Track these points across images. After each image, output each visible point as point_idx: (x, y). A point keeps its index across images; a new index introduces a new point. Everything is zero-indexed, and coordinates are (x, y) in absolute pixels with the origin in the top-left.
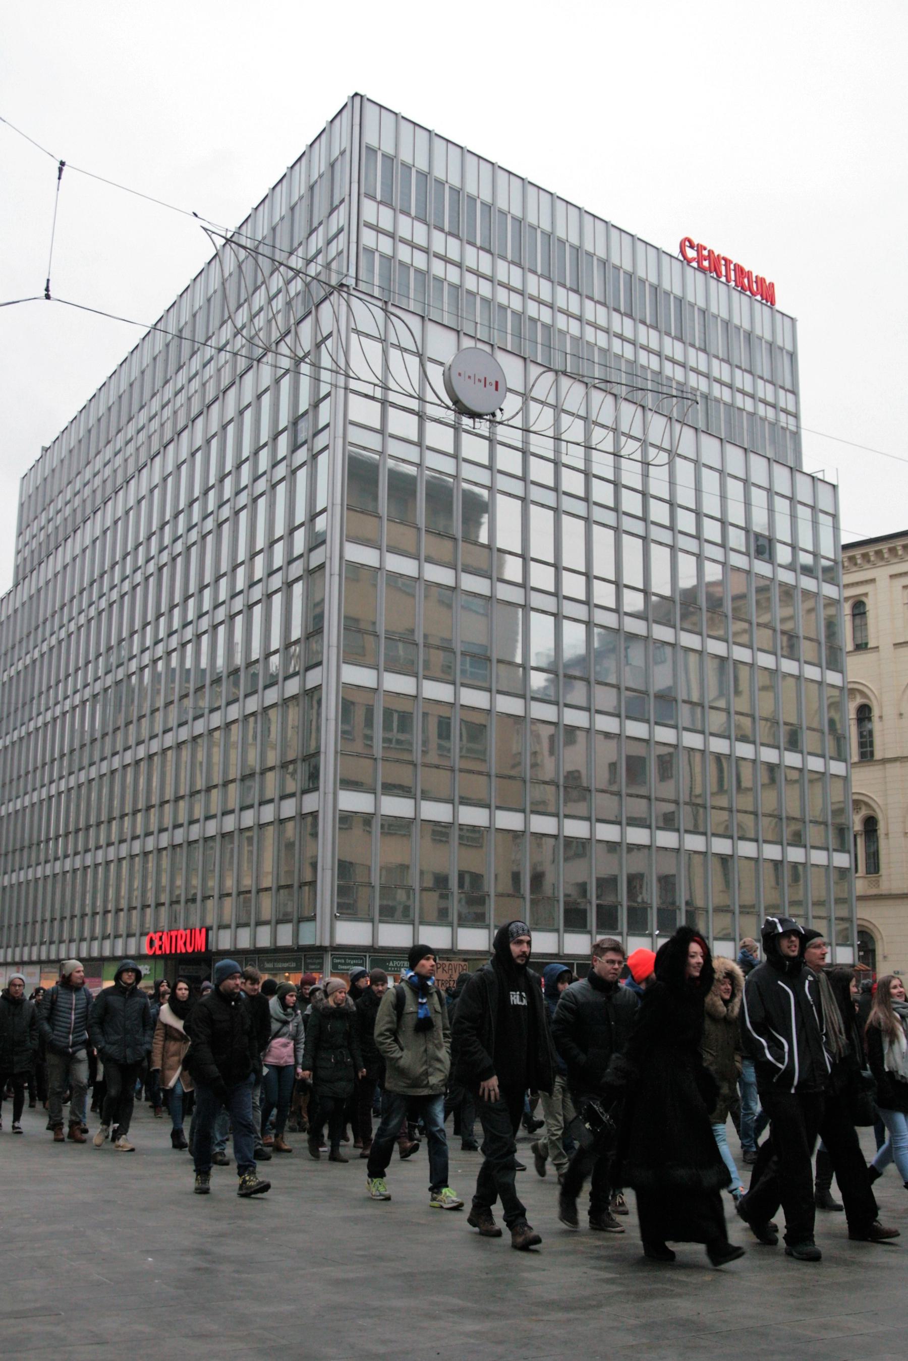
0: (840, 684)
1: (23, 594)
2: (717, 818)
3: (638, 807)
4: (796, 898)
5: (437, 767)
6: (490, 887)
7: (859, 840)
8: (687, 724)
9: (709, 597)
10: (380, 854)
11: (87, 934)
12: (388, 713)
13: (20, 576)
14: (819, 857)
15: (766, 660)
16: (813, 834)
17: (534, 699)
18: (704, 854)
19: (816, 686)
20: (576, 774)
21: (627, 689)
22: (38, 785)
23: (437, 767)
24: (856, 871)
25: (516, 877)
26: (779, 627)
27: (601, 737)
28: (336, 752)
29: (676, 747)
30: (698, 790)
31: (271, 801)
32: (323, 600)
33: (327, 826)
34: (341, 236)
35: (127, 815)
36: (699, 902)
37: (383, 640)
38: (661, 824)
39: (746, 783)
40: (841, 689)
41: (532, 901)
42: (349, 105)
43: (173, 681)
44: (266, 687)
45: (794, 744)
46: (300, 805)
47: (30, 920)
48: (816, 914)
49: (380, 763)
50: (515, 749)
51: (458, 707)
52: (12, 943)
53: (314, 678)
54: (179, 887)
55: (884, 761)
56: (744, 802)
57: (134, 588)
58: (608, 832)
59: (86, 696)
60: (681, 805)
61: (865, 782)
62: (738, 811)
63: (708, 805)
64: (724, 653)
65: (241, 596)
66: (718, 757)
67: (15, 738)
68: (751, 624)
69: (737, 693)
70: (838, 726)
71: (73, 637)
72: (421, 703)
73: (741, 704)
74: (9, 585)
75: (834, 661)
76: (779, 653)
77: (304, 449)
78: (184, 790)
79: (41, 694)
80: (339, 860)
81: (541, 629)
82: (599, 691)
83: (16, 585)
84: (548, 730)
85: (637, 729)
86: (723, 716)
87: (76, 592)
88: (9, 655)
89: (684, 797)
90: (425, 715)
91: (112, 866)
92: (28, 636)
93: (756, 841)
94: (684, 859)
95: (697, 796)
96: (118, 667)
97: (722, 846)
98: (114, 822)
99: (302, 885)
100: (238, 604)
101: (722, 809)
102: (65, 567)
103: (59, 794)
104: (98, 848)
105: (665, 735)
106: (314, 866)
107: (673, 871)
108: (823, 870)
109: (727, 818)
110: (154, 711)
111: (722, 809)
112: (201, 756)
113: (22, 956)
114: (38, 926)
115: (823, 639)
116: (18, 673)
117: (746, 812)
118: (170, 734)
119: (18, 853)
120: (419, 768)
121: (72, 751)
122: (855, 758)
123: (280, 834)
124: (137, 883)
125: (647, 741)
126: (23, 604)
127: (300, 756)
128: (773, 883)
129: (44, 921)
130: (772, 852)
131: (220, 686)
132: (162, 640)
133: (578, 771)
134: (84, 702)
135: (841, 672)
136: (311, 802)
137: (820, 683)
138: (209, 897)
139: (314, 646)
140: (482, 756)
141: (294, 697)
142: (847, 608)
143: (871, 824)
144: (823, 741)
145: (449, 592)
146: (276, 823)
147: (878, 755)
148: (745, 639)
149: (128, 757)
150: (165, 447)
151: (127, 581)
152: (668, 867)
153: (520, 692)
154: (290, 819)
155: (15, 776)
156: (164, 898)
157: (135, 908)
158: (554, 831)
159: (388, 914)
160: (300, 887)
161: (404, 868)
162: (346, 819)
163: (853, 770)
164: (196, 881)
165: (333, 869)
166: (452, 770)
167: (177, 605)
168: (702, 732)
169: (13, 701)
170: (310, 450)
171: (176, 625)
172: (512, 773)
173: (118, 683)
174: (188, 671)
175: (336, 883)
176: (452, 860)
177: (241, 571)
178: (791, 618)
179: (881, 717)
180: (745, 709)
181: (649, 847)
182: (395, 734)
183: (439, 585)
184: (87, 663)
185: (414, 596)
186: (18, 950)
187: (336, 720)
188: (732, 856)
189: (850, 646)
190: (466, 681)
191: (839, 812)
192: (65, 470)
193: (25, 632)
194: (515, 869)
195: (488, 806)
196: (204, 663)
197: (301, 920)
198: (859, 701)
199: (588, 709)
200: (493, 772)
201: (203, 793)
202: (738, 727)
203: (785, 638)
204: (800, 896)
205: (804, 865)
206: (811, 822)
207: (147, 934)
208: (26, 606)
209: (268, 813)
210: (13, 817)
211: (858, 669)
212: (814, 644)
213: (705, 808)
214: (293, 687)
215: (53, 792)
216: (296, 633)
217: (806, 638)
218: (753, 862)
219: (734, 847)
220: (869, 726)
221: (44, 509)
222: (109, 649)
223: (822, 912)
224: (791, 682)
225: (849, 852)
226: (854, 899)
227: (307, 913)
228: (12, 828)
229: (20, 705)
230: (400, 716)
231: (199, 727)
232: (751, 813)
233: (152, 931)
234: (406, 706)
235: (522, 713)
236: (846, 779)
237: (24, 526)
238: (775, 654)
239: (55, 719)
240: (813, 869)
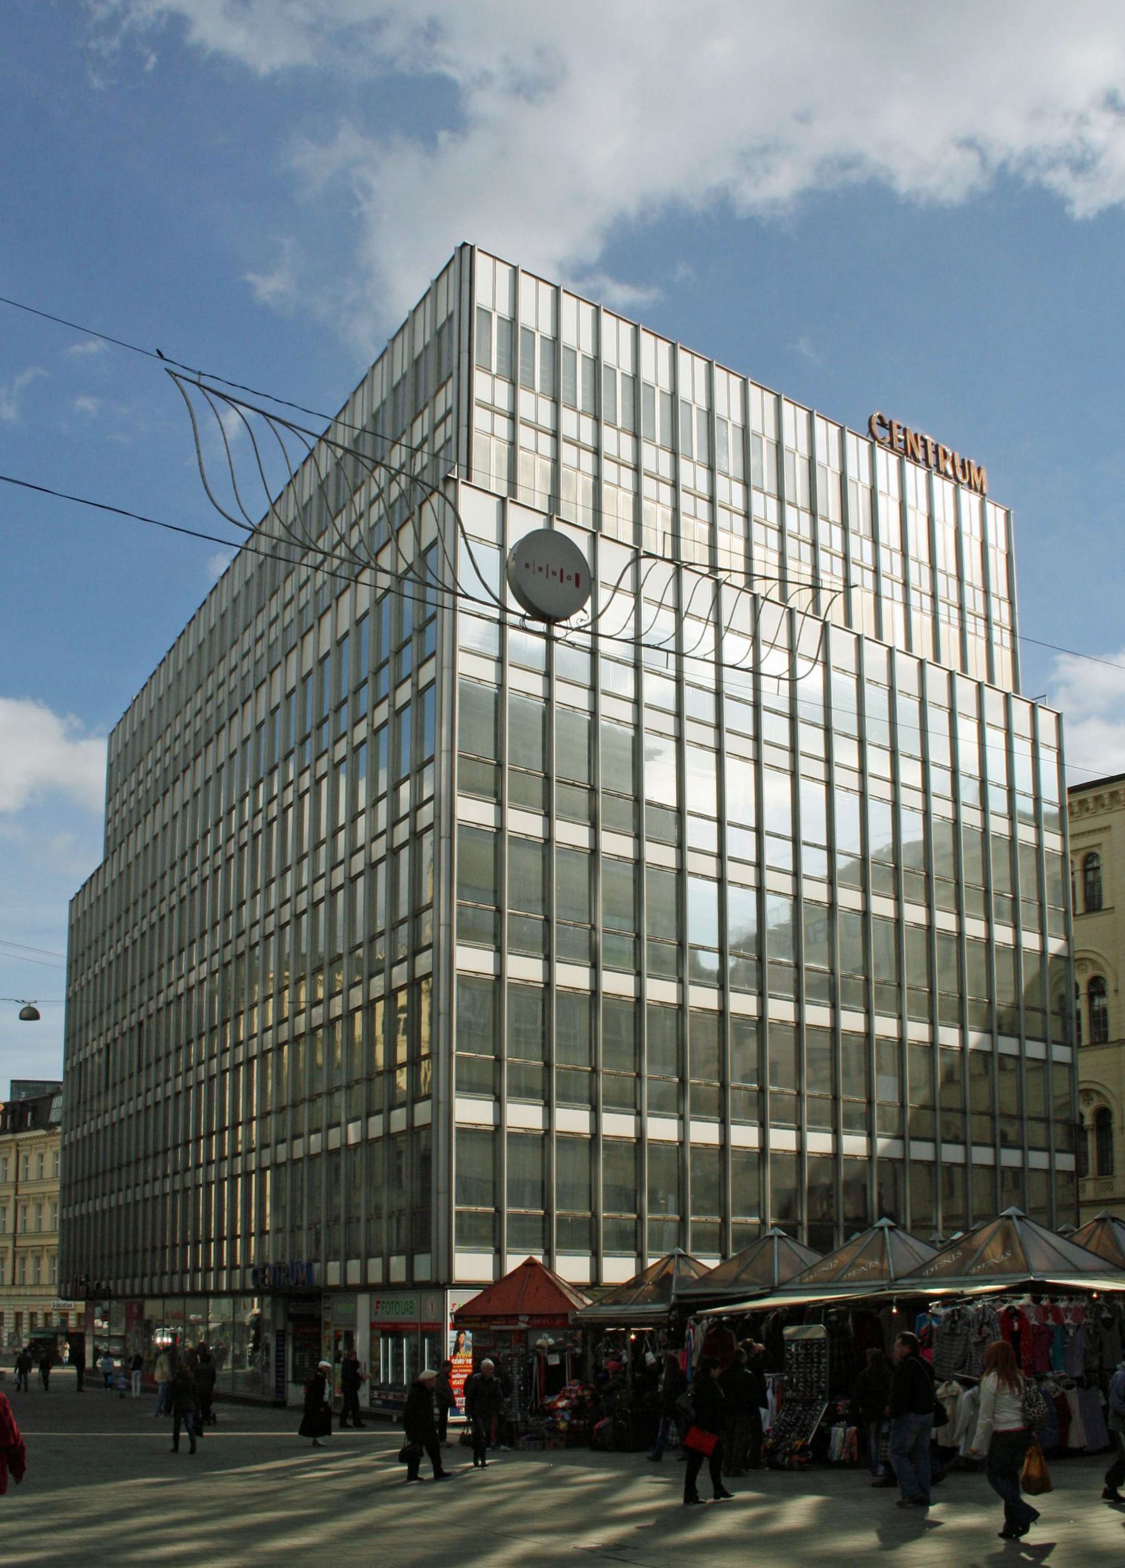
1: (112, 873)
14: (1039, 1160)
28: (438, 1054)
34: (449, 419)
42: (432, 291)
59: (228, 958)
61: (1093, 1066)
65: (342, 867)
74: (99, 860)
77: (407, 685)
83: (105, 861)
91: (179, 1196)
102: (196, 794)
113: (124, 1289)
130: (982, 1156)
143: (1103, 1116)
147: (1112, 1037)
150: (337, 599)
167: (323, 842)
169: (105, 998)
170: (415, 684)
177: (361, 821)
179: (1116, 991)
192: (146, 735)
221: (133, 770)
229: (137, 981)
232: (958, 1111)
236: (1072, 1067)
237: (114, 791)
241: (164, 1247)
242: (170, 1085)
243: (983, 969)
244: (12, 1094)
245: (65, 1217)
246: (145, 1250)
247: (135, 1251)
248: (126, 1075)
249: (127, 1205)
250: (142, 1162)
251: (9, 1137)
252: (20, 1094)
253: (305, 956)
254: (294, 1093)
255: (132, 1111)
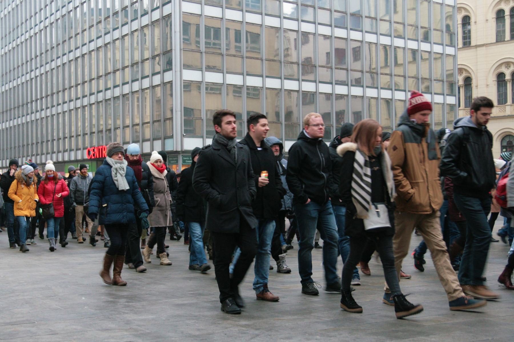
28: (181, 49)
147: (473, 43)
179: (475, 22)
232: (402, 76)
236: (454, 57)
241: (28, 145)
242: (33, 73)
246: (32, 144)
248: (8, 71)
250: (16, 109)
253: (85, 13)
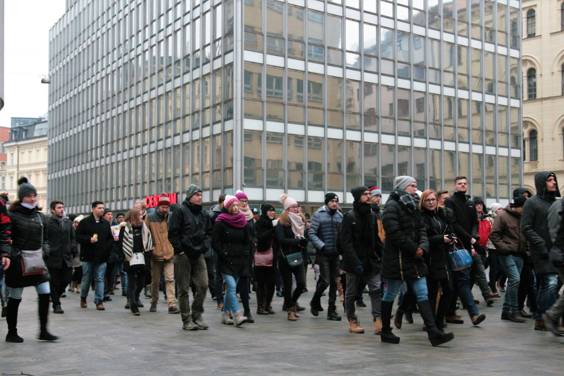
0: (518, 56)
2: (447, 132)
3: (404, 126)
4: (489, 175)
5: (296, 105)
6: (325, 169)
7: (526, 143)
8: (433, 80)
9: (445, 10)
10: (267, 154)
11: (114, 198)
12: (270, 78)
13: (69, 6)
14: (503, 152)
15: (476, 44)
16: (501, 139)
17: (348, 68)
18: (440, 151)
19: (504, 58)
20: (373, 110)
21: (399, 62)
22: (85, 120)
23: (296, 105)
24: (524, 159)
25: (339, 166)
26: (483, 26)
27: (385, 88)
28: (242, 98)
29: (425, 93)
30: (437, 118)
31: (208, 125)
32: (233, 17)
33: (238, 138)
35: (133, 135)
36: (438, 177)
37: (266, 37)
38: (417, 135)
39: (464, 113)
40: (518, 59)
41: (347, 176)
43: (154, 63)
44: (204, 64)
45: (491, 91)
46: (223, 127)
47: (84, 191)
48: (501, 182)
49: (265, 103)
50: (339, 96)
51: (307, 73)
52: (75, 204)
53: (229, 58)
54: (162, 174)
55: (542, 99)
56: (463, 123)
57: (131, 11)
58: (388, 139)
60: (428, 124)
61: (530, 111)
62: (459, 127)
63: (443, 124)
64: (452, 41)
66: (449, 98)
67: (72, 96)
68: (468, 24)
69: (460, 63)
70: (516, 81)
71: (100, 39)
72: (287, 72)
73: (462, 69)
74: (64, 11)
75: (515, 45)
76: (484, 40)
78: (162, 121)
79: (84, 71)
80: (245, 157)
81: (352, 28)
82: (383, 63)
83: (67, 11)
84: (356, 86)
85: (404, 83)
86: (451, 76)
87: (100, 15)
88: (66, 50)
89: (430, 119)
90: (290, 79)
92: (75, 39)
93: (469, 143)
94: (429, 154)
95: (438, 121)
96: (125, 55)
97: (449, 146)
98: (133, 137)
99: (226, 169)
100: (188, 19)
101: (450, 126)
103: (97, 125)
104: (118, 152)
105: (419, 86)
106: (232, 160)
107: (423, 162)
108: (505, 159)
109: (453, 132)
110: (145, 79)
111: (450, 126)
112: (171, 103)
114: (89, 194)
115: (509, 32)
116: (71, 60)
117: (463, 128)
118: (146, 95)
119: (76, 157)
120: (286, 106)
121: (102, 101)
122: (526, 98)
123: (214, 143)
124: (139, 173)
125: (409, 90)
126: (72, 22)
127: (223, 101)
128: (478, 167)
129: (91, 192)
130: (477, 149)
131: (179, 65)
132: (147, 40)
133: (374, 109)
134: (107, 75)
135: (519, 50)
136: (229, 125)
137: (506, 56)
138: (177, 177)
139: (229, 41)
140: (320, 100)
141: (219, 69)
142: (524, 14)
143: (533, 134)
144: (507, 89)
145: (301, 11)
146: (211, 137)
147: (539, 96)
148: (465, 33)
149: (132, 104)
151: (127, 7)
152: (420, 158)
153: (340, 64)
154: (218, 135)
155: (73, 116)
156: (154, 178)
157: (139, 184)
158: (359, 139)
159: (273, 184)
160: (225, 170)
161: (279, 162)
162: (249, 135)
163: (524, 105)
164: (170, 171)
165: (241, 161)
166: (304, 107)
167: (155, 21)
168: (440, 85)
171: (155, 32)
172: (338, 109)
173: (125, 64)
174: (162, 58)
175: (243, 167)
176: (305, 156)
178: (491, 21)
179: (541, 75)
180: (464, 72)
181: (410, 147)
182: (274, 90)
183: (296, 6)
184: (108, 53)
185: (282, 14)
186: (79, 208)
187: (242, 81)
188: (455, 152)
189: (525, 36)
190: (311, 59)
191: (516, 128)
193: (74, 38)
194: (339, 161)
195: (323, 126)
196: (170, 54)
197: (225, 187)
198: (529, 66)
199: (377, 73)
200: (326, 108)
201: (172, 122)
202: (460, 82)
203: (488, 32)
204: (493, 174)
205: (495, 156)
206: (499, 133)
207: (145, 197)
208: (74, 23)
209: (207, 132)
210: (65, 141)
211: (528, 48)
212: (504, 35)
213: (441, 126)
214: (218, 64)
215: (93, 124)
216: (219, 34)
217: (499, 31)
218: (467, 155)
219: (456, 147)
220: (534, 80)
222: (120, 45)
223: (505, 182)
224: (491, 56)
225: (520, 149)
226: (522, 174)
227: (229, 184)
228: (72, 143)
230: (275, 81)
231: (169, 87)
232: (466, 128)
233: (148, 196)
234: (278, 74)
235: (341, 76)
236: (519, 109)
238: (481, 40)
239: (92, 85)
240: (501, 159)
242: (93, 121)
243: (506, 165)
244: (12, 124)
245: (49, 179)
247: (87, 193)
249: (82, 172)
251: (14, 143)
252: (15, 124)
254: (166, 119)
255: (84, 128)
